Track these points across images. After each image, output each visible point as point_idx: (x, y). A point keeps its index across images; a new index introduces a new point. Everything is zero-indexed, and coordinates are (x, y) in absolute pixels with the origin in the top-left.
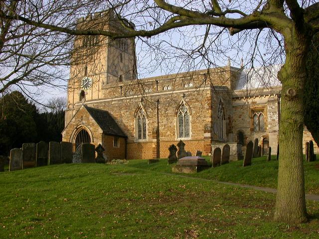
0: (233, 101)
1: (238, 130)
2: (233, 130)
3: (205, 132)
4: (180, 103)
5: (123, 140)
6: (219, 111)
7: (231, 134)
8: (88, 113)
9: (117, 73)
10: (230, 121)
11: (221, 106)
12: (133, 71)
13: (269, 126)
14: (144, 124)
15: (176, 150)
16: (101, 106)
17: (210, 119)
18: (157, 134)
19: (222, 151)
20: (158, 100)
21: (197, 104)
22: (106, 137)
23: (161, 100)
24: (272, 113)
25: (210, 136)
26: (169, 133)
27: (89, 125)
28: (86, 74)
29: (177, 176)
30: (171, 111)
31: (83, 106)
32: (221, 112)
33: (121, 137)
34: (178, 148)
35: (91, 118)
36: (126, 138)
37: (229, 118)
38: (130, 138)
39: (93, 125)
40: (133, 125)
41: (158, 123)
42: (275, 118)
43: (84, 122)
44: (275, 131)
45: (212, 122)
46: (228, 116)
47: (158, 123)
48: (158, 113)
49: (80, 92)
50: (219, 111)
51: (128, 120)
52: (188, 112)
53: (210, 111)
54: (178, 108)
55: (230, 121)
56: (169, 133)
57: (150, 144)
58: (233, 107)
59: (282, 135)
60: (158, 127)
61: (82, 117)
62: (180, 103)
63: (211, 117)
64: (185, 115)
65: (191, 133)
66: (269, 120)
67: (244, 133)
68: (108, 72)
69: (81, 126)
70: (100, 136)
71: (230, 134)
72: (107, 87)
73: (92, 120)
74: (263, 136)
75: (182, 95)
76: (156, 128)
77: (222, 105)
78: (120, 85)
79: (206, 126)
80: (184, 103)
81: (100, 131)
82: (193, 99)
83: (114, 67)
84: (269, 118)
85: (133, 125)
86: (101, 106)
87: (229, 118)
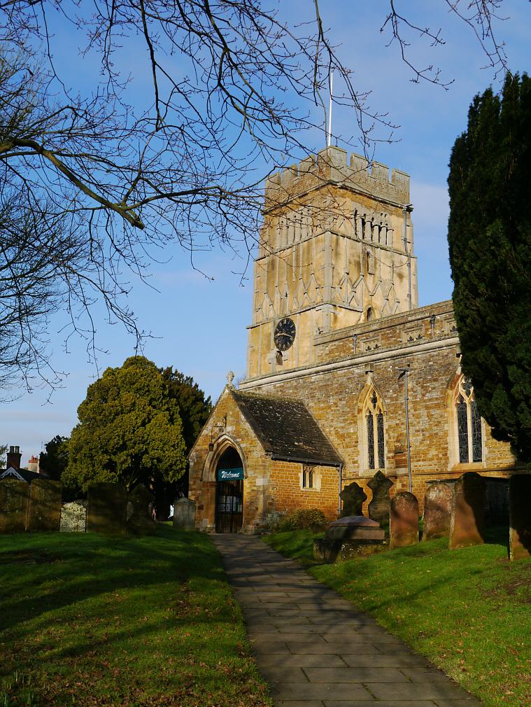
34: (368, 492)
86: (289, 388)
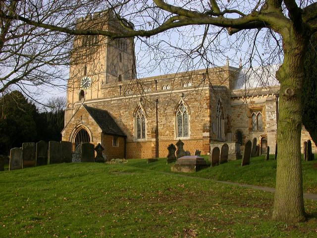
0: (232, 101)
1: (236, 129)
2: (232, 129)
3: (204, 132)
4: (179, 103)
5: (122, 139)
6: (218, 111)
7: (230, 133)
8: (88, 113)
9: (116, 72)
10: (229, 121)
11: (219, 106)
12: (133, 71)
13: (268, 125)
14: (143, 123)
15: (175, 149)
16: (100, 106)
17: (209, 118)
18: (156, 133)
19: (220, 150)
20: (157, 100)
21: (196, 103)
22: (106, 136)
23: (160, 100)
24: (270, 113)
25: (209, 136)
26: (168, 132)
27: (88, 124)
28: (85, 74)
29: (176, 175)
30: (170, 110)
31: (82, 106)
32: (220, 111)
33: (120, 136)
34: (176, 147)
35: (90, 117)
36: (125, 137)
37: (228, 118)
38: (129, 138)
39: (92, 124)
40: (132, 125)
41: (157, 122)
42: (273, 117)
43: (83, 121)
44: (273, 131)
45: (210, 121)
46: (227, 116)
47: (157, 122)
48: (157, 112)
49: (80, 91)
50: (218, 111)
51: (127, 120)
52: (187, 111)
53: (209, 110)
54: (177, 108)
55: (229, 121)
56: (168, 132)
57: (149, 143)
58: (232, 106)
59: (280, 135)
60: (157, 126)
61: (81, 117)
62: (179, 103)
63: (210, 116)
64: (184, 115)
65: (190, 133)
66: (268, 119)
67: (242, 132)
68: (107, 72)
69: (81, 126)
70: (100, 135)
71: (228, 134)
72: (107, 87)
73: (91, 119)
74: (261, 136)
75: (181, 95)
76: (155, 127)
77: (221, 105)
78: (119, 85)
79: (204, 126)
80: (183, 102)
81: (100, 130)
82: (192, 99)
83: (113, 67)
84: (267, 118)
85: (132, 125)
86: (100, 106)
87: (228, 118)
